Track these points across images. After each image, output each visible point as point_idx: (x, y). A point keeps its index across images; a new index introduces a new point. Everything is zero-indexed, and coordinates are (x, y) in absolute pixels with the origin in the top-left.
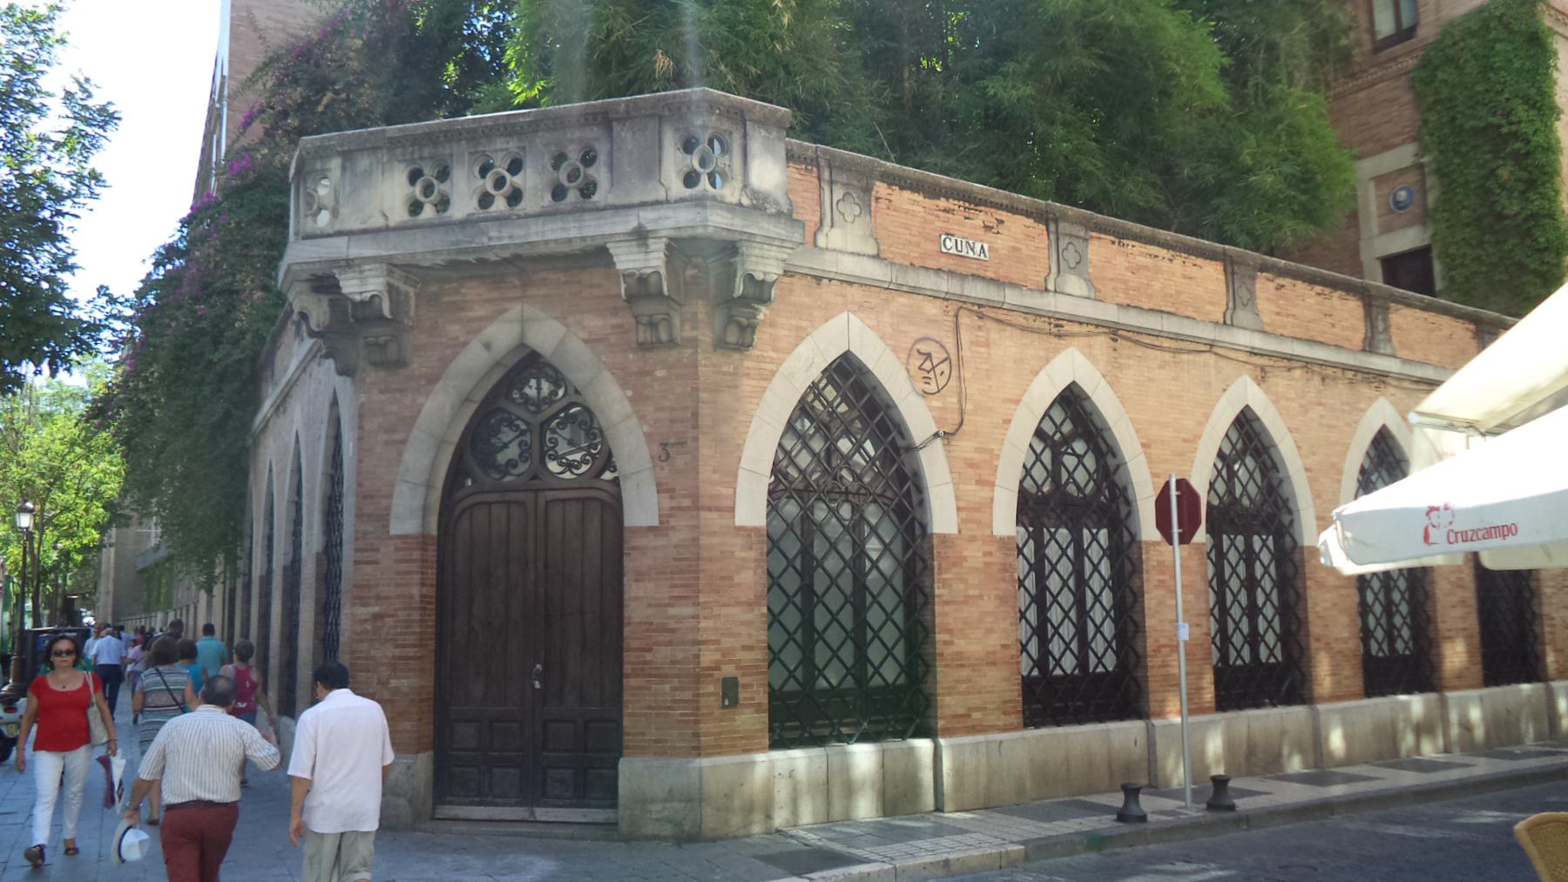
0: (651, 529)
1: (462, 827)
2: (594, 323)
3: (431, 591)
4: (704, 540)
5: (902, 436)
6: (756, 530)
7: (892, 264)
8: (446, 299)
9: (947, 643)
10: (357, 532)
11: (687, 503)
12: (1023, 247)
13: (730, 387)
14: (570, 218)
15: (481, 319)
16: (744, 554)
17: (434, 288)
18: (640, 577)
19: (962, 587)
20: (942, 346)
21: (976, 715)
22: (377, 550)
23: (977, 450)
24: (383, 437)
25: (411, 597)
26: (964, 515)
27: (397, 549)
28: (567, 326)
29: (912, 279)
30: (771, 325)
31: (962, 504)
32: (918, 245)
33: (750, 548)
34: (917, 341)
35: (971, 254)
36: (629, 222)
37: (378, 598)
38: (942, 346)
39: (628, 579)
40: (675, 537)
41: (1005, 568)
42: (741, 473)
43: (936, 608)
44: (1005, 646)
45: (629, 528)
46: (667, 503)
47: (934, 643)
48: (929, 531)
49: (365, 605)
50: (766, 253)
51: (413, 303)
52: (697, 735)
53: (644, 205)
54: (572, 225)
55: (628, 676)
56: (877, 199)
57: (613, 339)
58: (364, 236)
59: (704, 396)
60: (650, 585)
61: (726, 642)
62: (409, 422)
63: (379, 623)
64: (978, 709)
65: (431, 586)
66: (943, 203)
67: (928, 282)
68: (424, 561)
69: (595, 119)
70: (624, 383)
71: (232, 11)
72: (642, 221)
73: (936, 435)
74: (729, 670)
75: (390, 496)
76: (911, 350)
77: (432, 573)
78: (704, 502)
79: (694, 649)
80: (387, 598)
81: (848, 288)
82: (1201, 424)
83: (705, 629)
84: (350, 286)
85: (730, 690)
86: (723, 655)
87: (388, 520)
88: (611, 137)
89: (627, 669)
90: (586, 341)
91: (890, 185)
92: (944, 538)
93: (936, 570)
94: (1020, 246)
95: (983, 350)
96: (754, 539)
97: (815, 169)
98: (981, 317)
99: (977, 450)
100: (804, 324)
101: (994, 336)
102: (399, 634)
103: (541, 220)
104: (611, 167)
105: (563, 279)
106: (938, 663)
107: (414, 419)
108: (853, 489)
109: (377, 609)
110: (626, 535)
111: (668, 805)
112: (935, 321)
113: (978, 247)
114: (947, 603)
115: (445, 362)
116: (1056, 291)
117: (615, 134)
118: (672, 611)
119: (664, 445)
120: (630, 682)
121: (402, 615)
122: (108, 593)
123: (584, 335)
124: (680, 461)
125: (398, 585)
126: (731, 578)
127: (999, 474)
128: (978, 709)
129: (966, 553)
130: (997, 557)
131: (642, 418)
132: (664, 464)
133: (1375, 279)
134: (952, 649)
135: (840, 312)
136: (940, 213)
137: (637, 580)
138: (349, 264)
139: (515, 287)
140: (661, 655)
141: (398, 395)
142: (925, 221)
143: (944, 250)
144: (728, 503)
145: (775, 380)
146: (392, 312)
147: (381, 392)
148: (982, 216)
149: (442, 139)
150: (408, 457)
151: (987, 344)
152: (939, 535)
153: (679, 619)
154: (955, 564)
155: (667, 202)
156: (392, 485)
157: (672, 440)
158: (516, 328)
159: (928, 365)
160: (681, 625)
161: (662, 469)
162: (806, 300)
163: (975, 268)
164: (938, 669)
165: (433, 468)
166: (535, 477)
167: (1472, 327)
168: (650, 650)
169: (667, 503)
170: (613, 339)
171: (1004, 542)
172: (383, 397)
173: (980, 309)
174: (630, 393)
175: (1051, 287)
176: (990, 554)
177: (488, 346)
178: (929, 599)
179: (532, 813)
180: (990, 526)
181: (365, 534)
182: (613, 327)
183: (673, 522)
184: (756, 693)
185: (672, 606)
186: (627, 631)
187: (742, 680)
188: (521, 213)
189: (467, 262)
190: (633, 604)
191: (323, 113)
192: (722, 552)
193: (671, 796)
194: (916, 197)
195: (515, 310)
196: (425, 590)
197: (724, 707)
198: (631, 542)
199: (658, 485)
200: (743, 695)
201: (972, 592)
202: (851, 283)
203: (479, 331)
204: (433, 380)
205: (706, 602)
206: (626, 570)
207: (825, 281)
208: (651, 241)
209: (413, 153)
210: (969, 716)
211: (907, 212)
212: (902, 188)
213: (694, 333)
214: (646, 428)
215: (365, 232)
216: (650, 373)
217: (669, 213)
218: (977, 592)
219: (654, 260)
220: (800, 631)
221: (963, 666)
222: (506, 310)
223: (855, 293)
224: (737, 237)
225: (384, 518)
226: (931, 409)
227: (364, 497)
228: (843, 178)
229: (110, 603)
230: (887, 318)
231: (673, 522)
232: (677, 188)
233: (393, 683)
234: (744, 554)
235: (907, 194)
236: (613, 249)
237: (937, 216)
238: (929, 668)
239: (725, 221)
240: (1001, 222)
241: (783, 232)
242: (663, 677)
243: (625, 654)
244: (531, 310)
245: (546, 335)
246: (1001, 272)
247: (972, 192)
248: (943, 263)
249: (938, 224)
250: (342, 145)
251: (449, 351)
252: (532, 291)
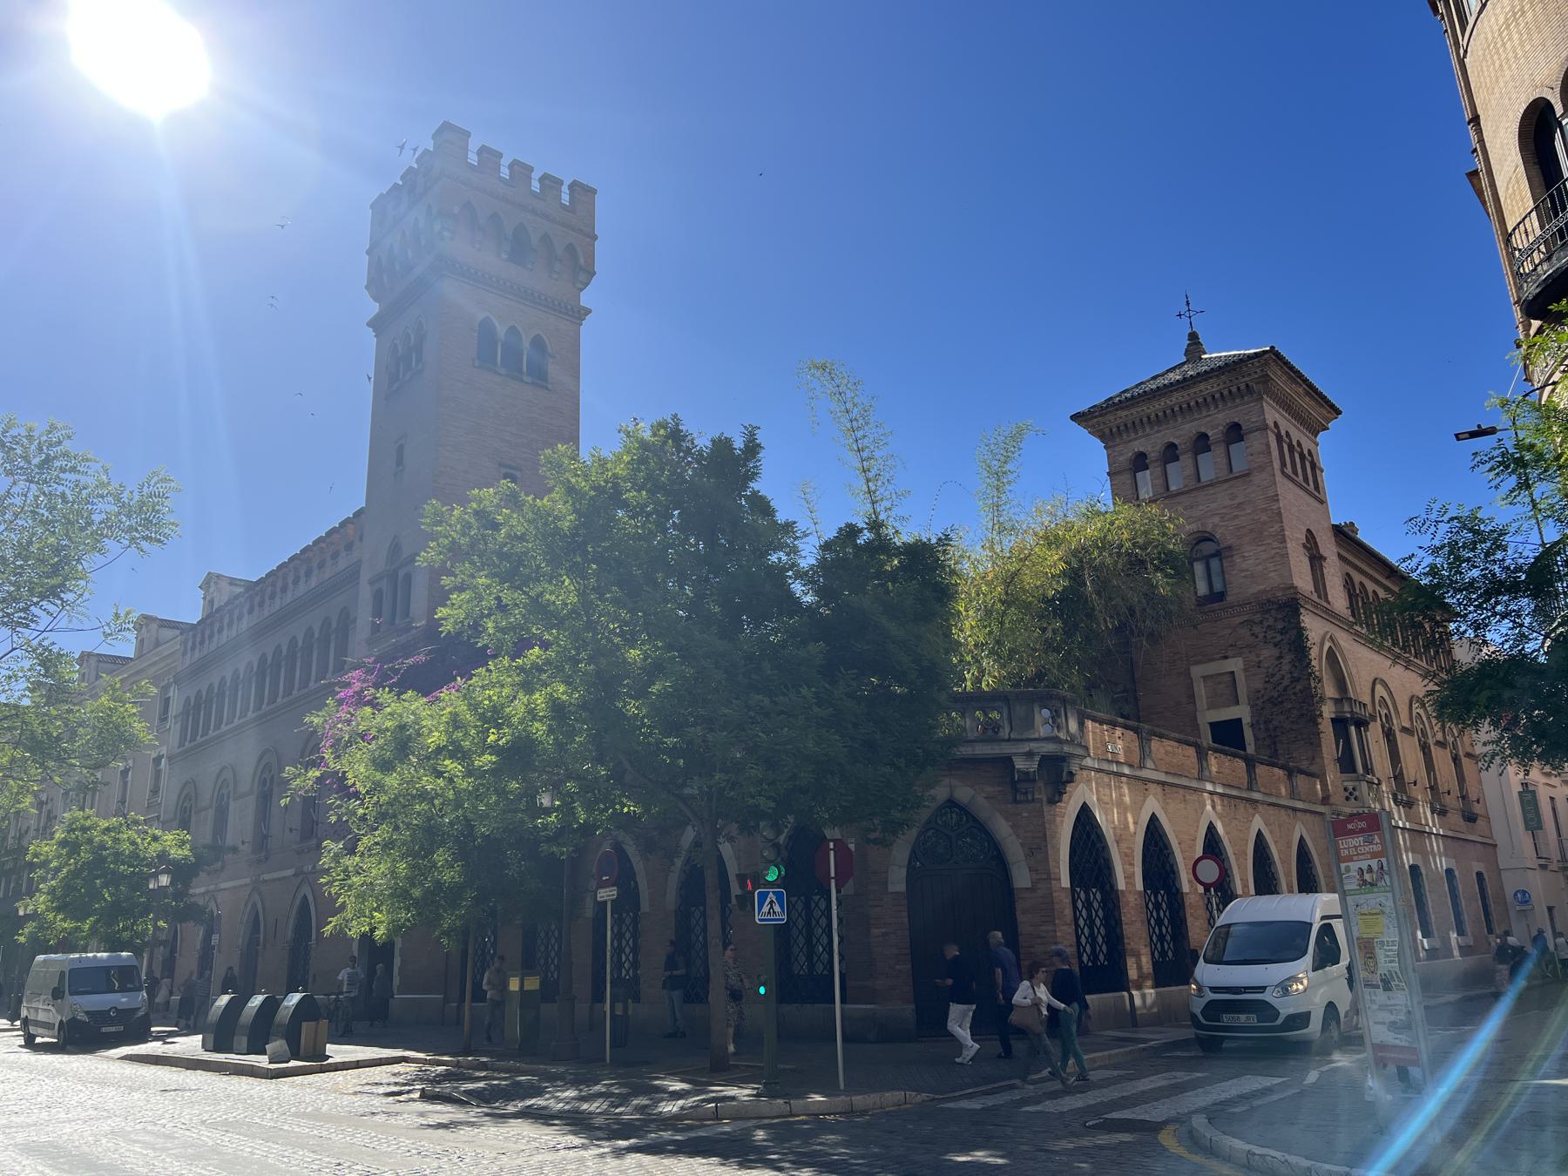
2: (989, 789)
11: (1045, 876)
28: (975, 790)
36: (1026, 747)
42: (1061, 862)
59: (1047, 826)
78: (1052, 876)
82: (1196, 831)
90: (985, 798)
92: (1122, 891)
99: (1127, 848)
118: (1042, 928)
123: (985, 795)
133: (1207, 739)
167: (1286, 773)
179: (1185, 453)
182: (999, 791)
183: (1039, 886)
185: (1041, 925)
186: (1020, 938)
213: (1040, 796)
214: (1020, 841)
217: (1044, 745)
219: (1033, 766)
231: (1039, 886)
236: (1014, 759)
245: (964, 794)
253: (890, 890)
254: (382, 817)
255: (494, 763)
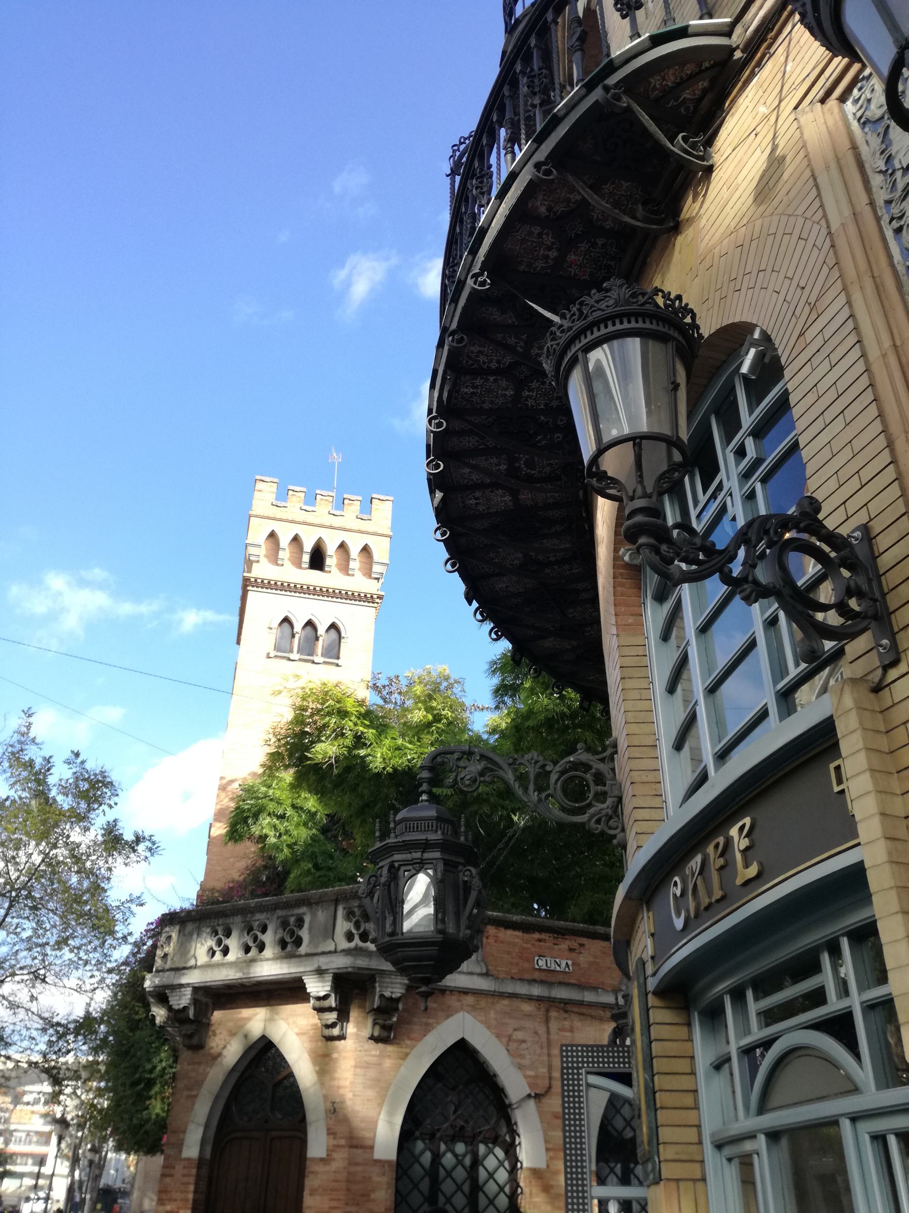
0: (322, 1160)
6: (389, 1162)
16: (378, 1179)
18: (313, 1192)
22: (174, 1168)
27: (185, 1167)
28: (288, 1024)
29: (510, 988)
32: (517, 964)
33: (384, 1175)
35: (558, 969)
39: (306, 1193)
46: (333, 1142)
50: (394, 981)
53: (323, 953)
60: (318, 1198)
67: (522, 989)
73: (529, 1096)
90: (297, 1034)
94: (598, 961)
95: (569, 1034)
98: (566, 1011)
110: (308, 1163)
113: (563, 964)
123: (297, 1030)
126: (369, 1195)
132: (332, 1116)
137: (311, 1195)
141: (196, 1066)
143: (537, 967)
146: (194, 1015)
147: (189, 1064)
148: (568, 942)
151: (571, 1030)
156: (186, 1125)
163: (561, 978)
166: (266, 1121)
172: (189, 1067)
173: (565, 1006)
183: (335, 1155)
192: (364, 1177)
199: (328, 1129)
207: (448, 992)
223: (470, 1000)
224: (374, 972)
226: (526, 1077)
230: (492, 1015)
234: (378, 1179)
235: (510, 932)
240: (582, 945)
246: (582, 979)
248: (537, 975)
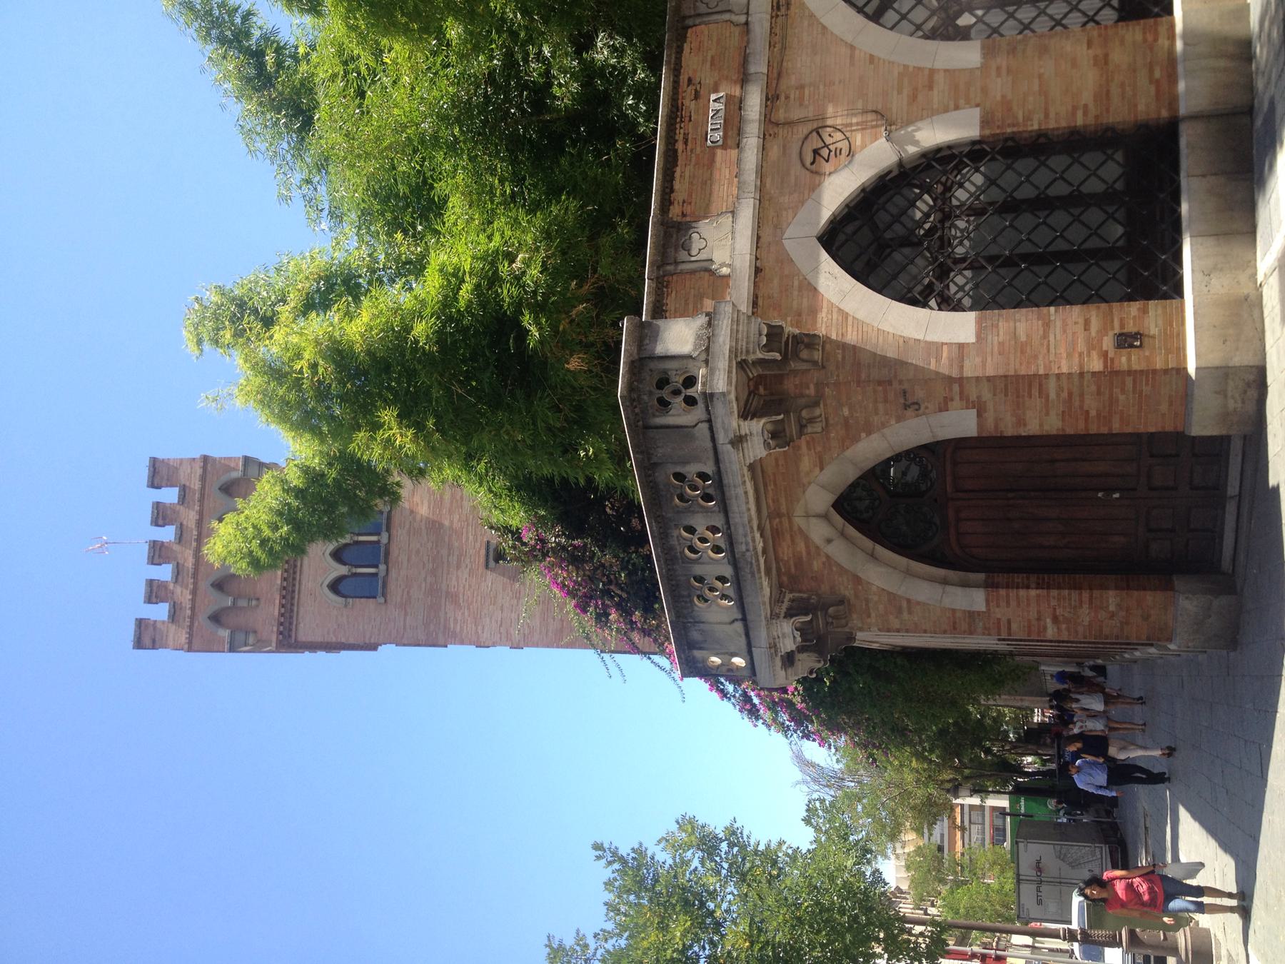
0: (979, 415)
1: (1242, 557)
2: (806, 463)
3: (1033, 578)
4: (990, 372)
5: (890, 172)
6: (979, 322)
7: (738, 198)
8: (793, 570)
9: (1085, 113)
10: (984, 634)
11: (956, 388)
12: (710, 54)
13: (855, 353)
14: (727, 494)
15: (807, 547)
17: (785, 579)
18: (1021, 422)
19: (1031, 99)
20: (806, 138)
21: (1157, 74)
22: (999, 620)
23: (900, 92)
24: (905, 616)
25: (1038, 596)
26: (962, 102)
28: (810, 483)
30: (800, 315)
31: (952, 106)
34: (803, 165)
37: (1039, 619)
38: (806, 138)
39: (1023, 432)
40: (987, 395)
41: (1012, 51)
42: (929, 339)
43: (1051, 127)
44: (1089, 44)
45: (978, 432)
46: (957, 402)
47: (1085, 126)
48: (978, 138)
49: (1045, 628)
51: (797, 595)
52: (1166, 371)
54: (733, 492)
55: (1110, 429)
56: (684, 215)
57: (819, 449)
58: (752, 636)
60: (1029, 414)
61: (1081, 346)
62: (892, 597)
63: (1061, 618)
64: (1151, 71)
65: (1028, 578)
66: (680, 146)
68: (1007, 587)
69: (650, 476)
70: (856, 439)
71: (553, 647)
72: (727, 441)
74: (1108, 343)
75: (954, 611)
76: (812, 172)
77: (1018, 578)
79: (1087, 377)
80: (1039, 612)
81: (762, 240)
83: (1070, 367)
84: (789, 645)
85: (1127, 340)
86: (1094, 349)
87: (974, 612)
88: (661, 464)
89: (1104, 430)
90: (822, 469)
91: (671, 203)
92: (985, 123)
93: (1015, 129)
94: (709, 58)
95: (807, 92)
96: (989, 323)
97: (666, 279)
99: (900, 92)
100: (796, 283)
101: (793, 80)
102: (1070, 604)
103: (731, 515)
104: (685, 462)
105: (772, 487)
106: (1105, 122)
107: (889, 593)
108: (939, 215)
109: (1048, 620)
111: (1230, 394)
112: (784, 147)
114: (1047, 115)
115: (843, 571)
116: (747, 13)
117: (660, 461)
118: (1053, 395)
119: (906, 407)
120: (1116, 427)
121: (1054, 603)
122: (1022, 700)
123: (817, 469)
124: (920, 393)
125: (1028, 605)
127: (921, 64)
128: (1151, 71)
129: (999, 98)
130: (1002, 61)
131: (884, 425)
134: (1091, 106)
135: (784, 249)
136: (689, 148)
137: (1025, 425)
138: (773, 646)
139: (781, 522)
140: (1092, 404)
142: (697, 163)
144: (955, 350)
145: (847, 310)
146: (806, 614)
147: (869, 616)
148: (687, 102)
149: (674, 583)
150: (921, 597)
151: (801, 87)
152: (982, 128)
153: (1060, 389)
154: (1010, 109)
155: (709, 421)
157: (902, 401)
158: (814, 520)
159: (825, 152)
160: (1066, 388)
161: (927, 408)
162: (776, 282)
164: (1111, 120)
165: (932, 579)
168: (1087, 412)
169: (957, 402)
170: (819, 449)
171: (988, 52)
172: (873, 615)
174: (863, 435)
175: (742, 19)
176: (998, 68)
177: (829, 541)
178: (1041, 134)
179: (1232, 497)
180: (972, 71)
181: (985, 628)
182: (809, 449)
183: (973, 397)
184: (1130, 314)
185: (1048, 396)
186: (1070, 431)
187: (1117, 331)
188: (725, 527)
189: (766, 561)
190: (1046, 428)
191: (628, 593)
193: (1223, 393)
194: (677, 175)
195: (799, 521)
196: (1033, 585)
197: (1141, 346)
198: (990, 429)
200: (1131, 328)
201: (1036, 88)
202: (759, 238)
203: (817, 548)
204: (857, 580)
205: (1045, 367)
206: (1015, 434)
208: (743, 433)
209: (686, 602)
210: (1158, 81)
211: (691, 183)
212: (672, 191)
214: (893, 422)
215: (747, 635)
216: (846, 420)
218: (1036, 82)
219: (756, 427)
220: (1071, 210)
221: (1108, 91)
222: (800, 529)
225: (971, 615)
227: (955, 628)
228: (671, 251)
229: (1031, 698)
232: (698, 412)
233: (1112, 608)
237: (692, 151)
238: (1110, 129)
239: (722, 377)
240: (690, 80)
241: (725, 322)
242: (1112, 401)
243: (1091, 432)
244: (799, 510)
245: (818, 497)
247: (665, 114)
249: (698, 149)
250: (684, 651)
251: (834, 569)
252: (783, 509)
253: (984, 609)
254: (503, 185)
255: (577, 484)
